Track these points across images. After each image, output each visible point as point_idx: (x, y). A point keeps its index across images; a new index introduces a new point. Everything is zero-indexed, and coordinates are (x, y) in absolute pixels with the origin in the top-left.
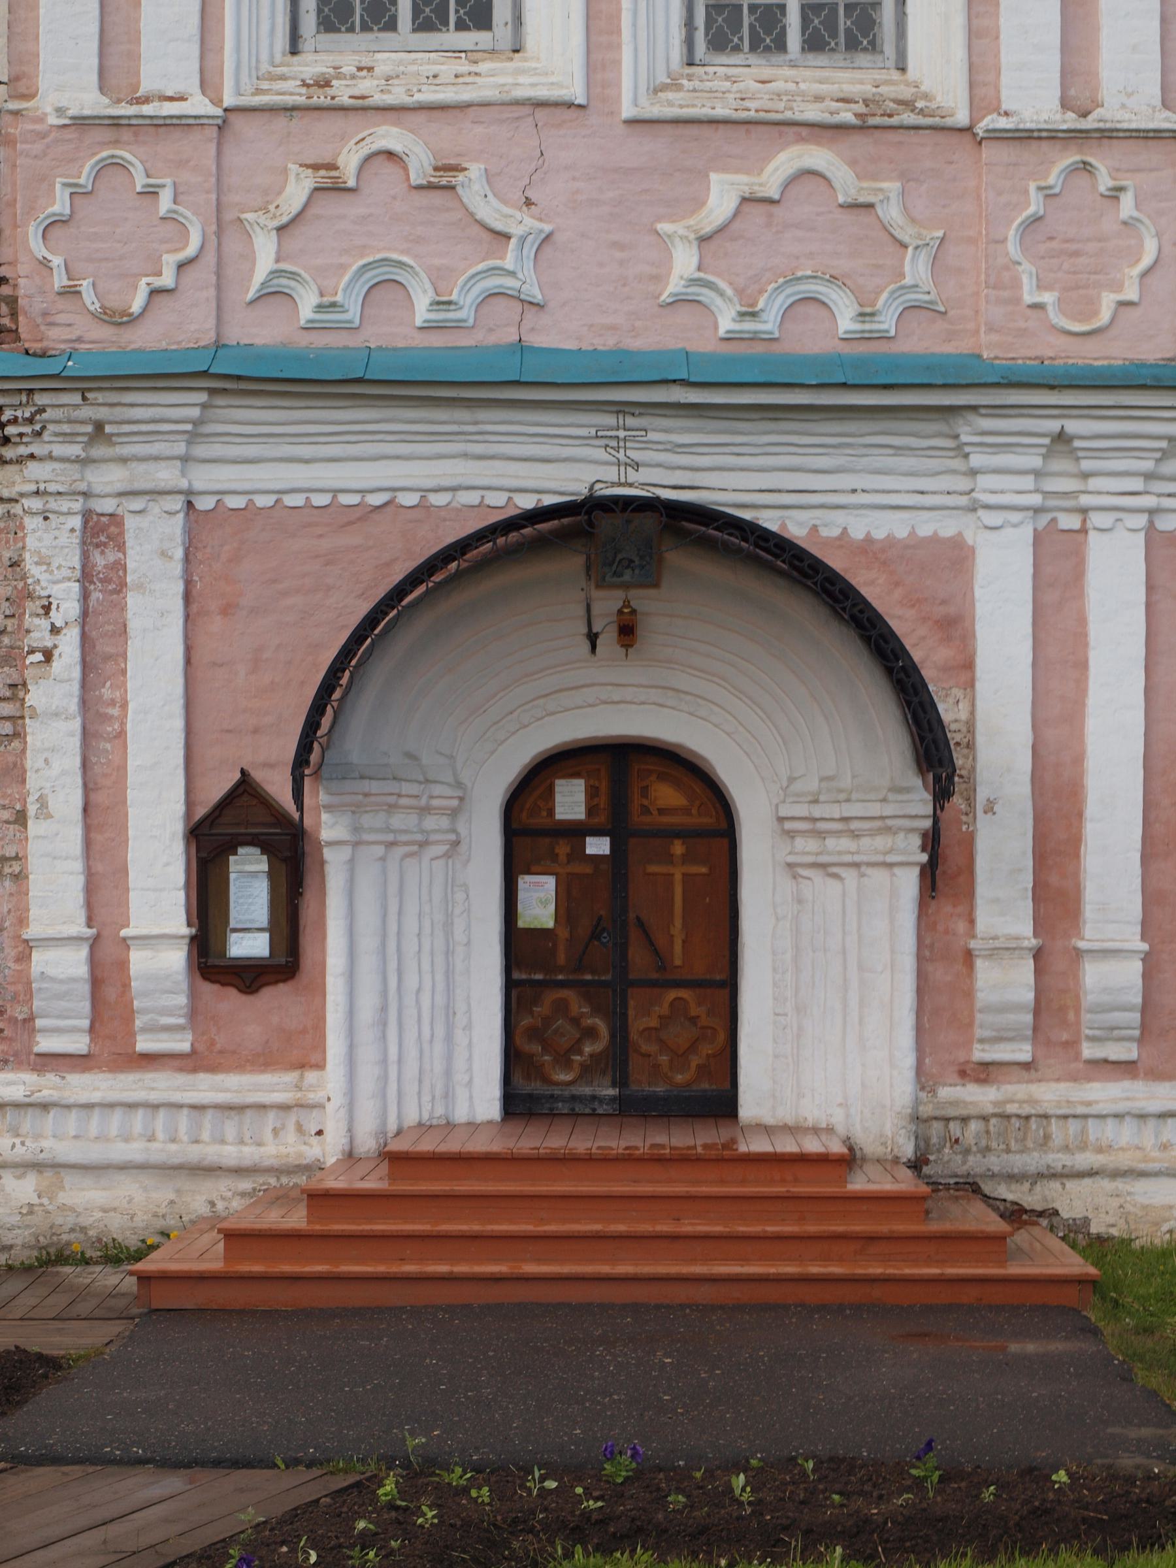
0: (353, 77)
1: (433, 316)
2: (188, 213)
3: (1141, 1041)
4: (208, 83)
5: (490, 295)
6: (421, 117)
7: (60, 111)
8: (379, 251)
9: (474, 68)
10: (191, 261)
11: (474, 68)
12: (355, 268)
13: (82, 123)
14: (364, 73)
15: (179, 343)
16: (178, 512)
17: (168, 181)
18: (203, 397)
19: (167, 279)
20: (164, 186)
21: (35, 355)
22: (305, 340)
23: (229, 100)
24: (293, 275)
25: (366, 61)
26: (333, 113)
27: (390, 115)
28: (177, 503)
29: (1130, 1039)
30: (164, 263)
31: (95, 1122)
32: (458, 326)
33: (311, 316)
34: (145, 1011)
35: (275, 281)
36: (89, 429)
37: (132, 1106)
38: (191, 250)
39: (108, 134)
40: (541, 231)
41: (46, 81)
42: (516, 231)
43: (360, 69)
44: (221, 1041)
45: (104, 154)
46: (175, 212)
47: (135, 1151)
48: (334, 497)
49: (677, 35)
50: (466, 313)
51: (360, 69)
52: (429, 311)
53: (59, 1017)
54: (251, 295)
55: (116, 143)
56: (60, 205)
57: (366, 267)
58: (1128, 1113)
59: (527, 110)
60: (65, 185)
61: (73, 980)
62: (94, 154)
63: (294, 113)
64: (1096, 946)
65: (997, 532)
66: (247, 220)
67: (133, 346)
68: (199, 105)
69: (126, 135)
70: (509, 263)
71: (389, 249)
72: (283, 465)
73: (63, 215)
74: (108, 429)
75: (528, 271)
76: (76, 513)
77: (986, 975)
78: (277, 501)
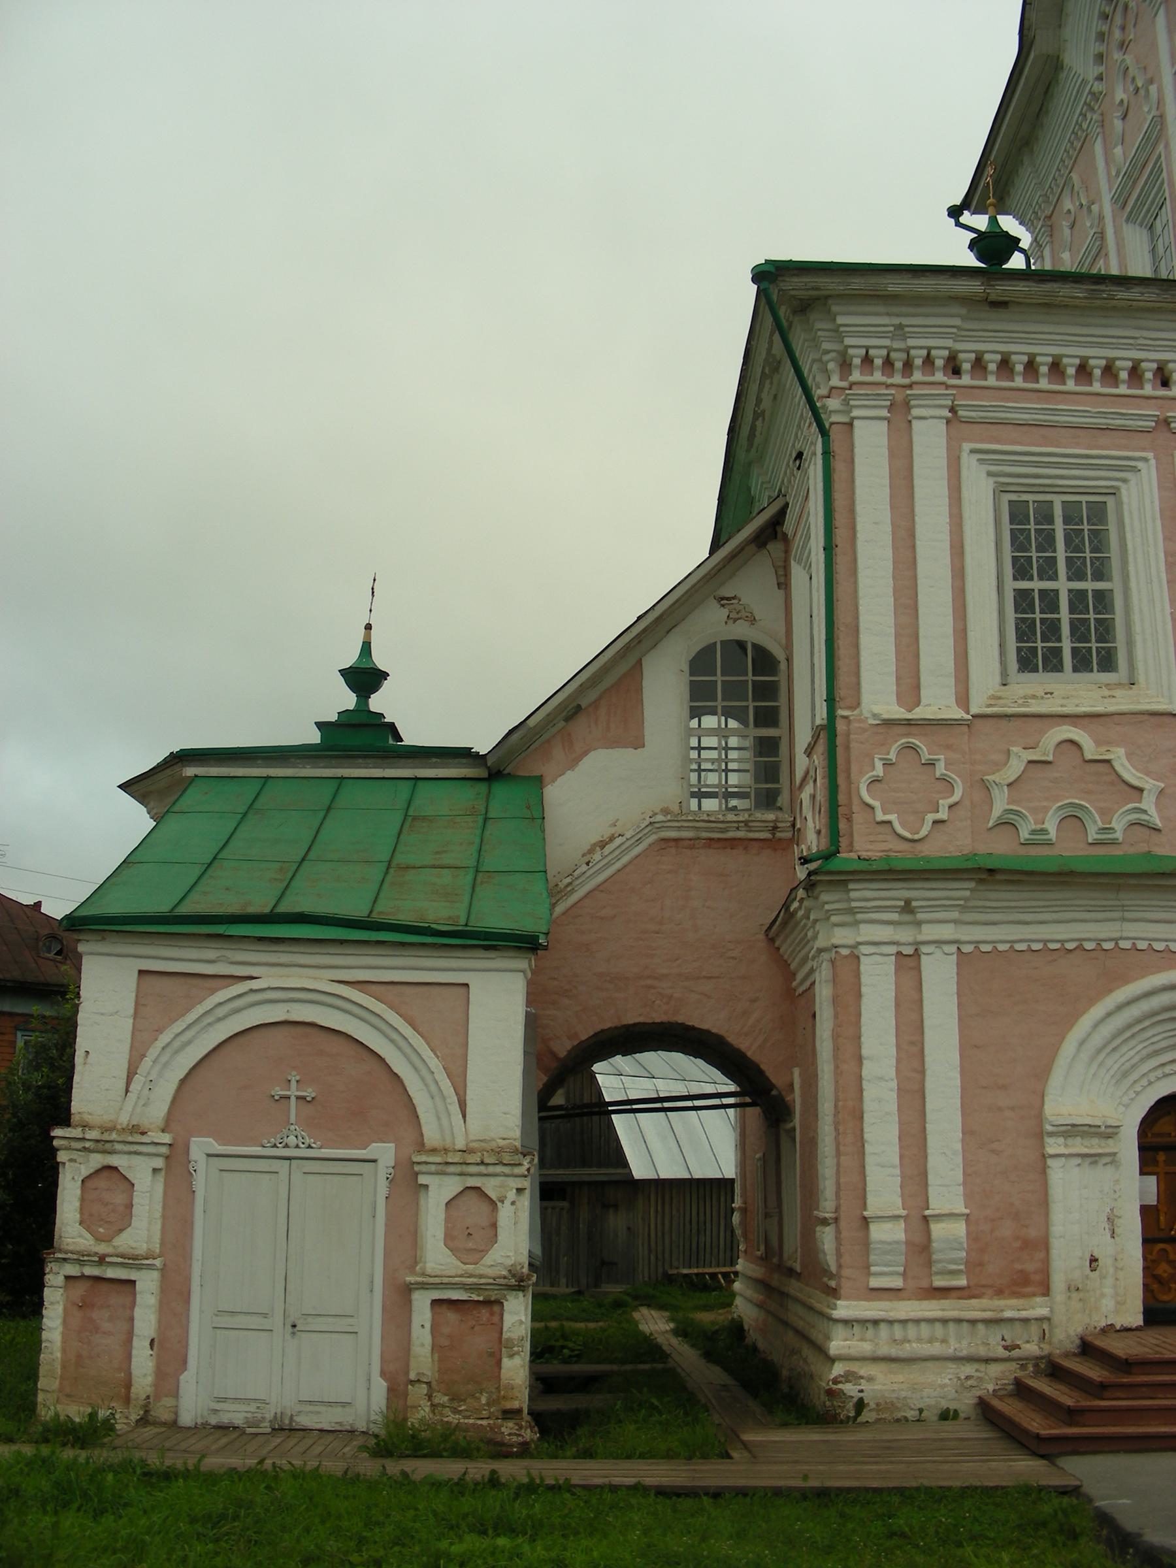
0: (1042, 698)
1: (1099, 837)
2: (953, 776)
3: (904, 1275)
4: (963, 700)
5: (1132, 824)
6: (1086, 721)
7: (875, 716)
8: (1067, 798)
9: (1111, 693)
10: (956, 804)
11: (1111, 693)
12: (1054, 808)
13: (889, 723)
14: (1049, 696)
15: (950, 852)
16: (953, 954)
17: (942, 757)
18: (972, 885)
19: (943, 815)
20: (939, 760)
21: (865, 859)
22: (1023, 851)
23: (974, 710)
24: (1017, 813)
25: (1049, 689)
26: (1034, 719)
27: (1067, 720)
28: (953, 948)
29: (897, 1273)
30: (940, 805)
31: (912, 1331)
32: (1113, 843)
33: (1028, 836)
34: (940, 1261)
35: (1006, 816)
36: (902, 903)
37: (917, 1321)
38: (956, 798)
39: (903, 730)
40: (1159, 787)
41: (866, 698)
42: (1146, 786)
43: (1046, 694)
44: (1037, 1278)
45: (903, 741)
46: (945, 775)
47: (936, 1349)
48: (1117, 944)
49: (996, 666)
50: (1119, 835)
51: (1046, 694)
52: (1097, 833)
53: (886, 1265)
54: (991, 824)
55: (908, 735)
56: (879, 770)
57: (1060, 808)
58: (883, 1320)
59: (1146, 717)
60: (880, 759)
61: (897, 1242)
62: (896, 741)
63: (1011, 718)
64: (937, 1212)
65: (929, 956)
66: (988, 780)
67: (923, 855)
68: (959, 714)
69: (913, 730)
70: (1143, 806)
71: (1073, 798)
72: (1013, 926)
73: (878, 776)
74: (914, 904)
75: (1152, 811)
76: (892, 955)
77: (877, 1232)
78: (1010, 948)
